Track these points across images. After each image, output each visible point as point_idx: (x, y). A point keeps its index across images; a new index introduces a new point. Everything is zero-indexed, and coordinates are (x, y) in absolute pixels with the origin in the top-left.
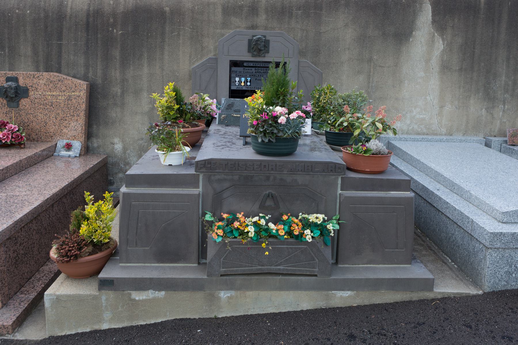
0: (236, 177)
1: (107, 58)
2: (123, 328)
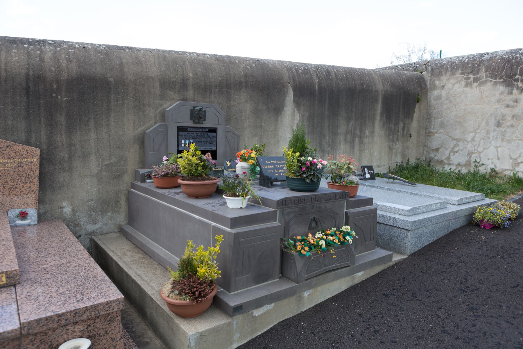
0: (297, 209)
1: (52, 124)
2: (248, 343)
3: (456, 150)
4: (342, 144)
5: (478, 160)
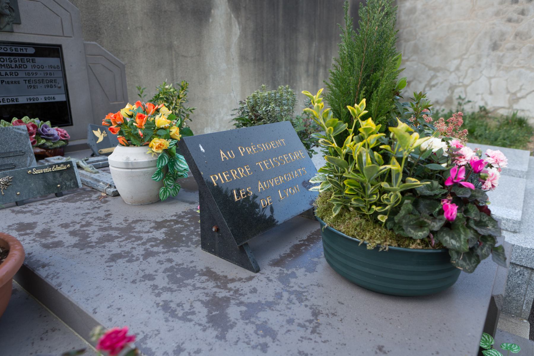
3: (433, 83)
4: (303, 79)
5: (463, 96)
